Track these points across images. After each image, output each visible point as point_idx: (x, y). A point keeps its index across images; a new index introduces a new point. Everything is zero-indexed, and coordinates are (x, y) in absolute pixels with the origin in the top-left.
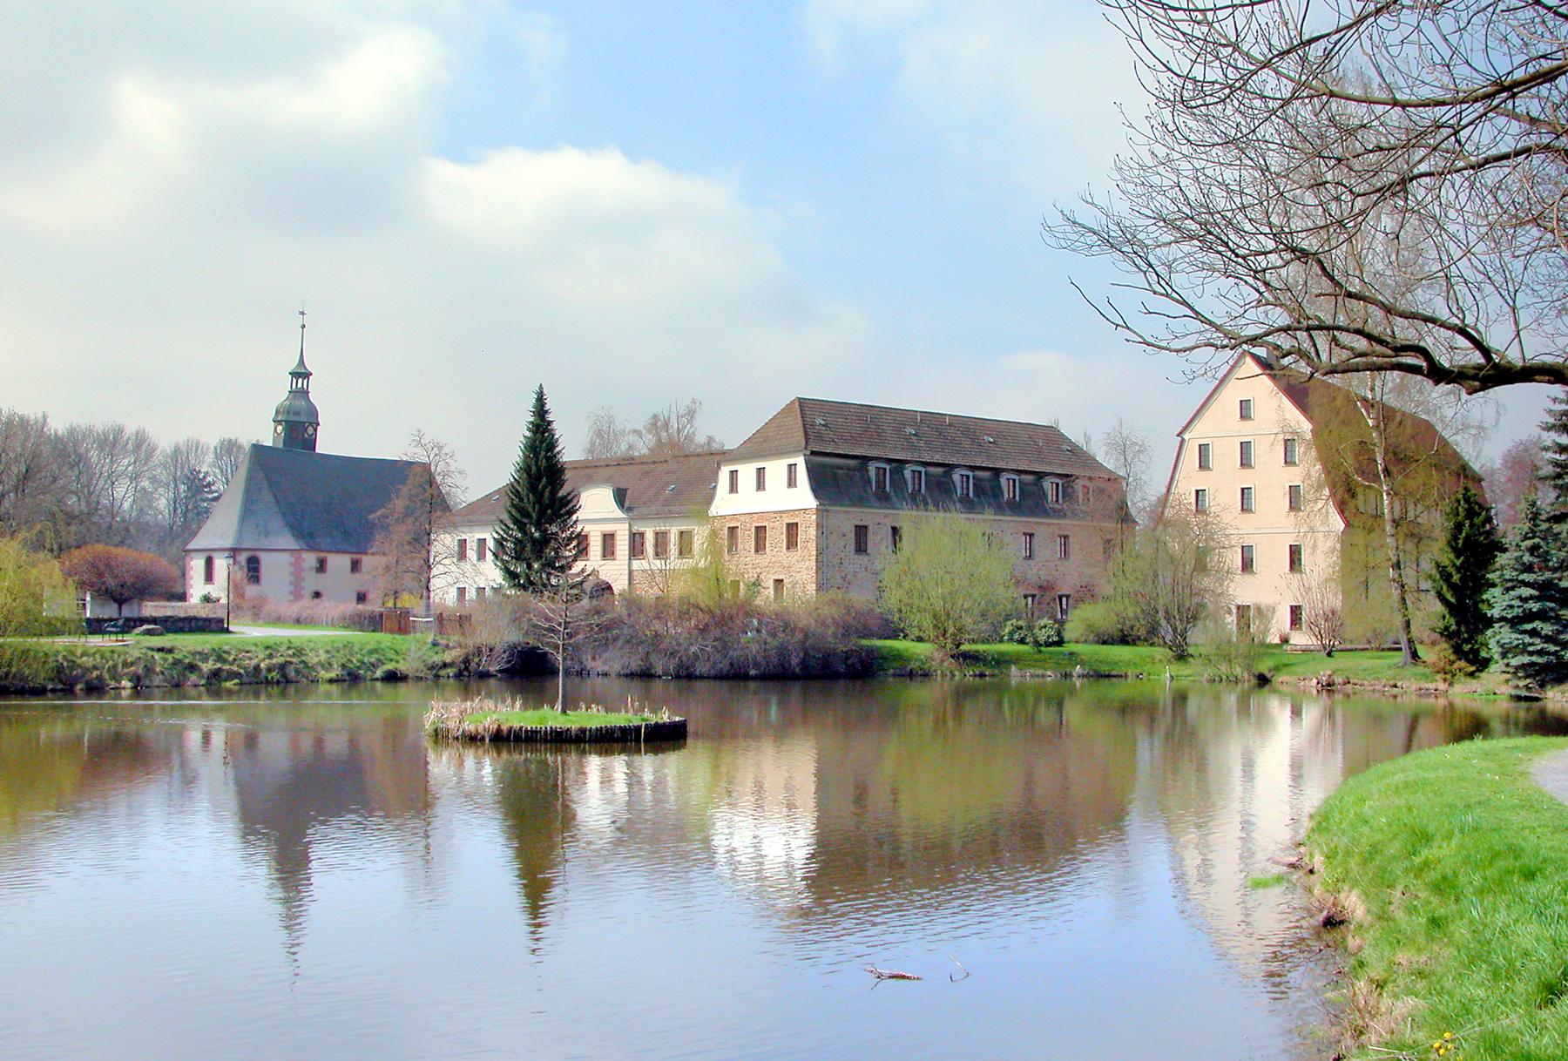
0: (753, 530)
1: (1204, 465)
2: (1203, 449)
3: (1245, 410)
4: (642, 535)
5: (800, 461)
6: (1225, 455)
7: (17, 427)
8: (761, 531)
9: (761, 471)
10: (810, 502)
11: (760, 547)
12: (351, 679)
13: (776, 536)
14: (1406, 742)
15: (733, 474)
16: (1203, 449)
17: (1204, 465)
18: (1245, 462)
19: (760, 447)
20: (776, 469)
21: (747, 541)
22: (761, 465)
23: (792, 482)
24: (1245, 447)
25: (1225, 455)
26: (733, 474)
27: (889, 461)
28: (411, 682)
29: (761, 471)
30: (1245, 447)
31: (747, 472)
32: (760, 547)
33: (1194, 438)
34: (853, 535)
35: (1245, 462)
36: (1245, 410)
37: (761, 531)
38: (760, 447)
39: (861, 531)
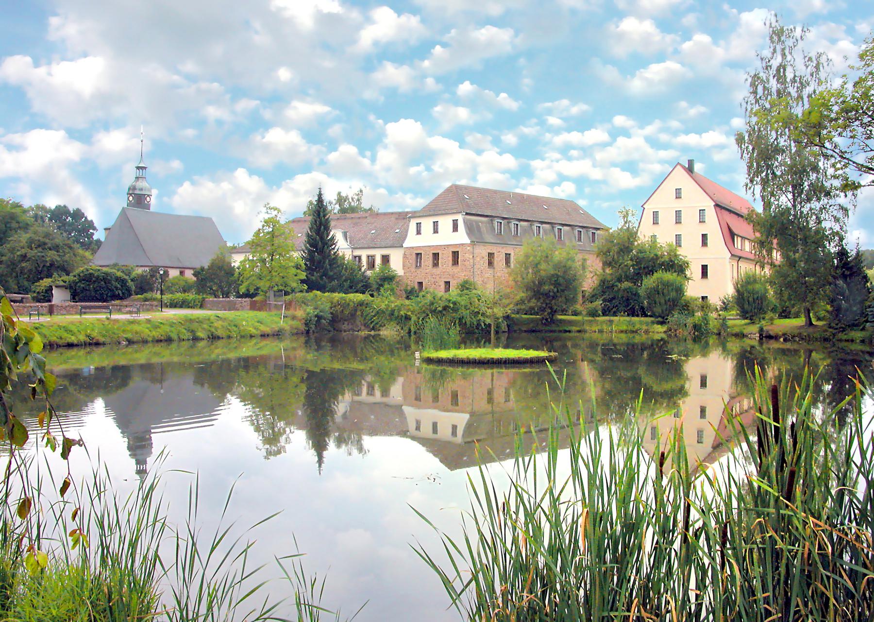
0: (431, 255)
1: (655, 222)
2: (655, 214)
3: (678, 194)
4: (360, 257)
5: (460, 218)
6: (667, 218)
7: (10, 195)
8: (436, 256)
9: (436, 224)
10: (466, 240)
11: (436, 264)
12: (852, 341)
13: (446, 259)
14: (486, 366)
15: (419, 225)
16: (655, 214)
17: (655, 222)
18: (678, 221)
19: (434, 209)
20: (445, 222)
21: (427, 260)
22: (435, 219)
23: (455, 228)
24: (678, 213)
25: (667, 218)
26: (419, 225)
27: (504, 218)
28: (150, 339)
29: (436, 224)
30: (678, 213)
31: (427, 224)
32: (436, 264)
33: (650, 207)
34: (487, 258)
35: (678, 221)
36: (678, 194)
37: (436, 256)
38: (434, 209)
39: (491, 255)
